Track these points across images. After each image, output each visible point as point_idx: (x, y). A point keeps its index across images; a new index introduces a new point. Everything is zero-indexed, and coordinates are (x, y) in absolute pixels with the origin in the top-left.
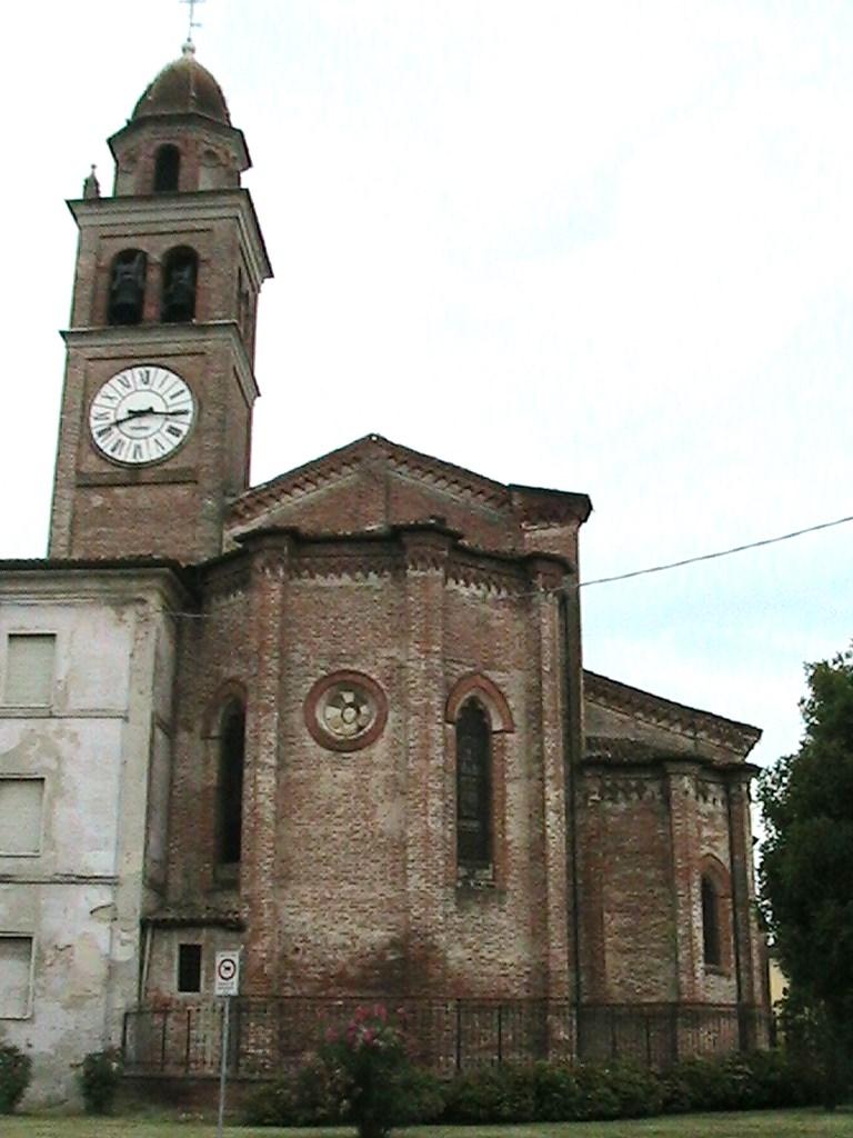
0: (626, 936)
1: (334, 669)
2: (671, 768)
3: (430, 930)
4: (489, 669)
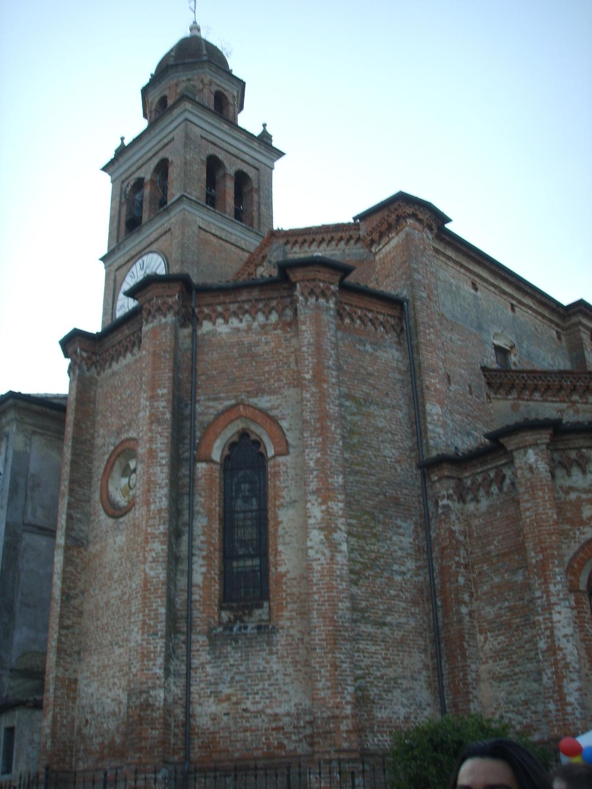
0: (501, 659)
1: (118, 442)
2: (511, 443)
3: (144, 687)
4: (256, 395)
